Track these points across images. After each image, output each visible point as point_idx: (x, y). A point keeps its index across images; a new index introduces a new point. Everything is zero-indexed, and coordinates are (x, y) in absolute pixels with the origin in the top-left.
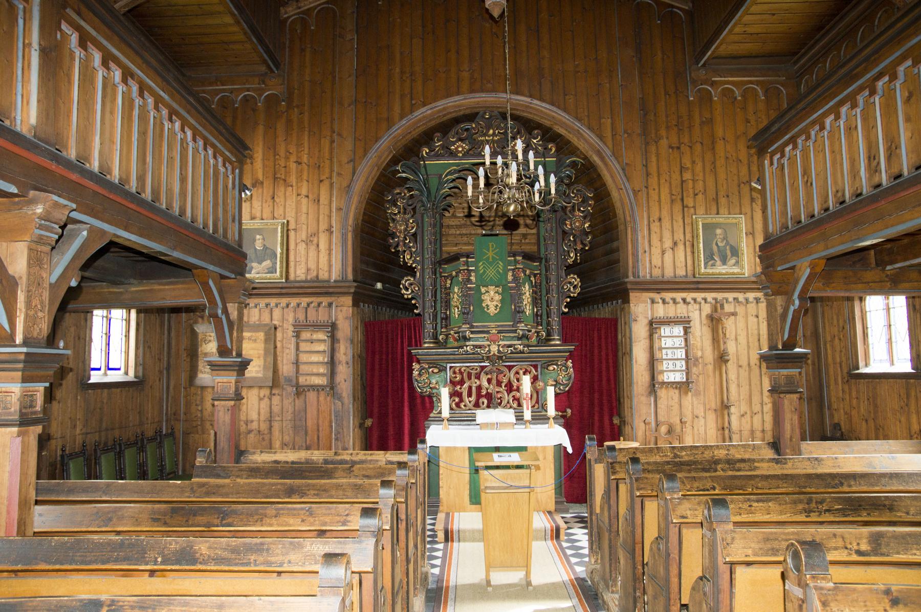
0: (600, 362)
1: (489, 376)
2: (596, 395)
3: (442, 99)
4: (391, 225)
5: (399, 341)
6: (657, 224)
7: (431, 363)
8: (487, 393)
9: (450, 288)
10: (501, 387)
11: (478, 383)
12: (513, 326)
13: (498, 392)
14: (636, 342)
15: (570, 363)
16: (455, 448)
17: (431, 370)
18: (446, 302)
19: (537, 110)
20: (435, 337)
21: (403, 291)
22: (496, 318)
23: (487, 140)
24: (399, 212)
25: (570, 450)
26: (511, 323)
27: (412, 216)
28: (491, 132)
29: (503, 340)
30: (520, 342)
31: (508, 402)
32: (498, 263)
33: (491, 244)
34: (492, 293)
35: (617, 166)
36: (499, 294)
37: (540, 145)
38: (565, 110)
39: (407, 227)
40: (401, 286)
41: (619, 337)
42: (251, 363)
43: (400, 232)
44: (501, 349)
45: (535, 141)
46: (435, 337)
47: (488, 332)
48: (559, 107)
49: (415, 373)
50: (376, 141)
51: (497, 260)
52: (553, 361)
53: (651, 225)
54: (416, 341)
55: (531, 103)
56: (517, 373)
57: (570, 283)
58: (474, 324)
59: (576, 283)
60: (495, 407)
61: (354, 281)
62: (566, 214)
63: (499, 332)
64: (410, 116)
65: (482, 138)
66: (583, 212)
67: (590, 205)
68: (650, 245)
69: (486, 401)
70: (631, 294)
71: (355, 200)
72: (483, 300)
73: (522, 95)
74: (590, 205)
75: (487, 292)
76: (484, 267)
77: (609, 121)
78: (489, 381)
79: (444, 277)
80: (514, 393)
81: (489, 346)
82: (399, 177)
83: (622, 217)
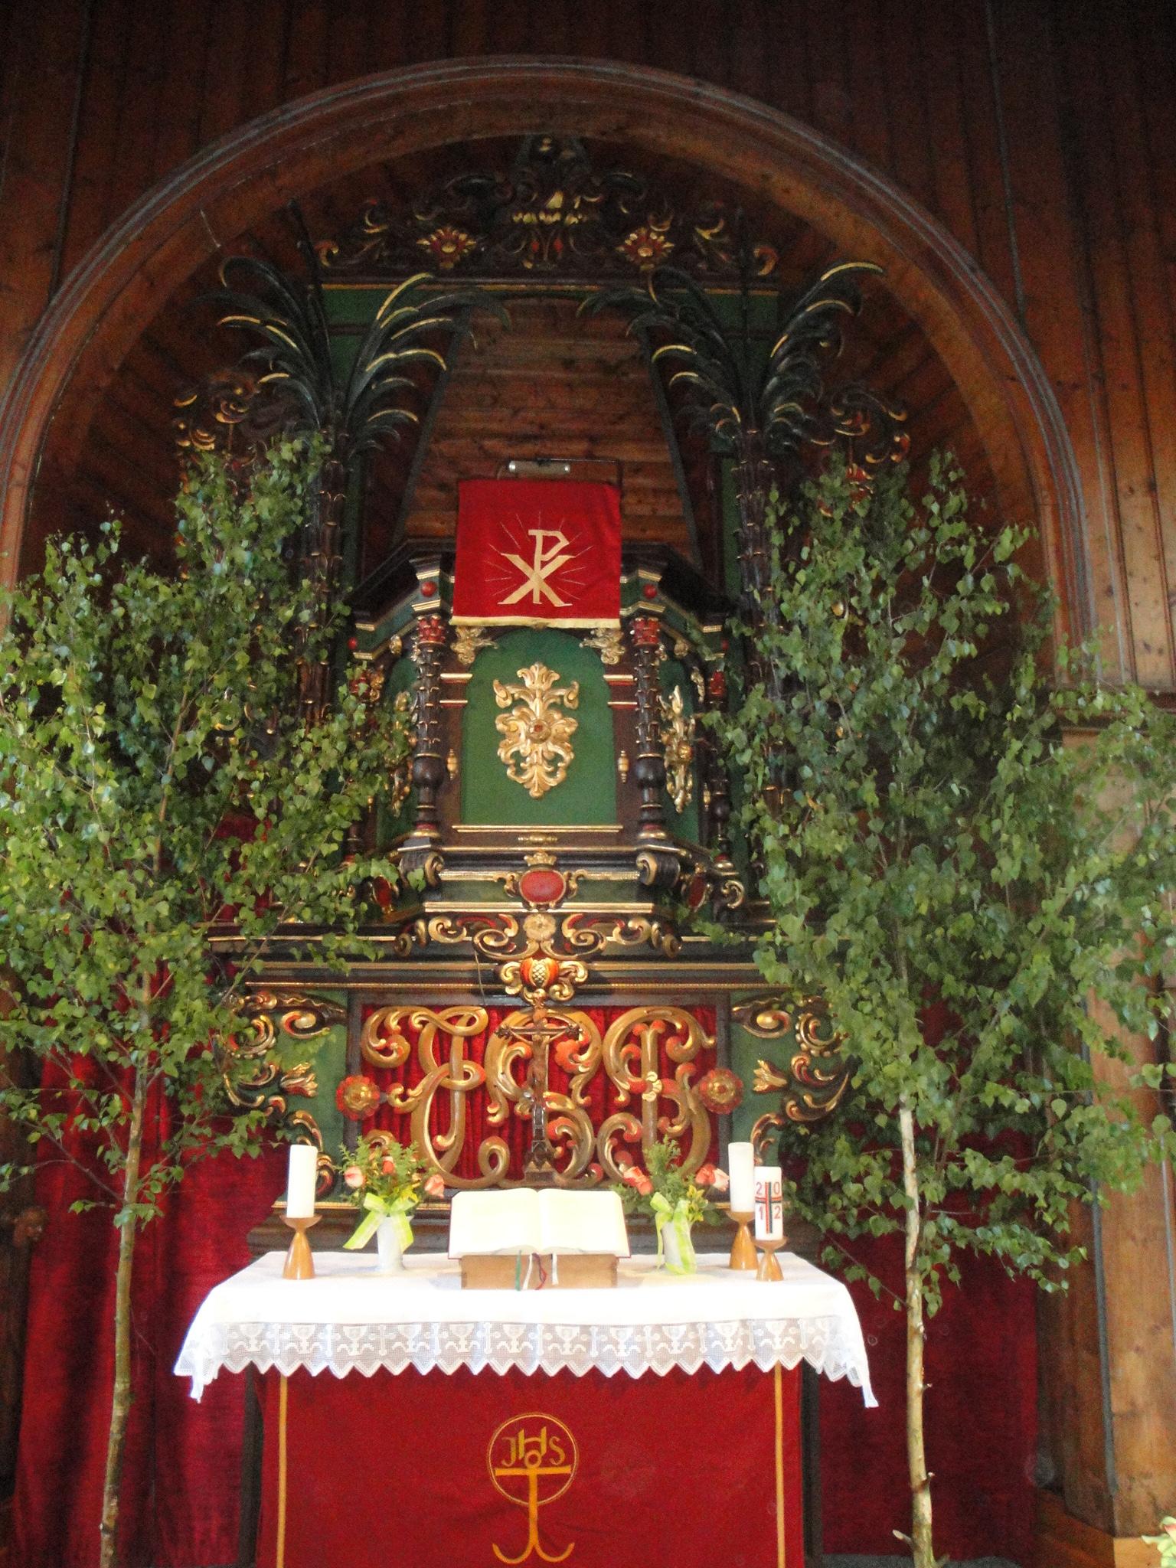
6: (1141, 499)
10: (569, 1093)
11: (475, 1078)
12: (618, 839)
13: (553, 1115)
22: (547, 807)
26: (614, 828)
28: (556, 201)
29: (580, 897)
30: (647, 907)
31: (595, 1158)
34: (536, 706)
37: (722, 247)
42: (1164, 976)
44: (569, 933)
45: (706, 235)
47: (513, 860)
53: (1122, 500)
55: (696, 95)
56: (631, 1038)
58: (462, 829)
60: (541, 1182)
63: (566, 861)
64: (276, 112)
67: (897, 448)
68: (1124, 572)
71: (52, 381)
72: (502, 736)
74: (897, 448)
75: (518, 703)
78: (519, 1067)
81: (520, 918)
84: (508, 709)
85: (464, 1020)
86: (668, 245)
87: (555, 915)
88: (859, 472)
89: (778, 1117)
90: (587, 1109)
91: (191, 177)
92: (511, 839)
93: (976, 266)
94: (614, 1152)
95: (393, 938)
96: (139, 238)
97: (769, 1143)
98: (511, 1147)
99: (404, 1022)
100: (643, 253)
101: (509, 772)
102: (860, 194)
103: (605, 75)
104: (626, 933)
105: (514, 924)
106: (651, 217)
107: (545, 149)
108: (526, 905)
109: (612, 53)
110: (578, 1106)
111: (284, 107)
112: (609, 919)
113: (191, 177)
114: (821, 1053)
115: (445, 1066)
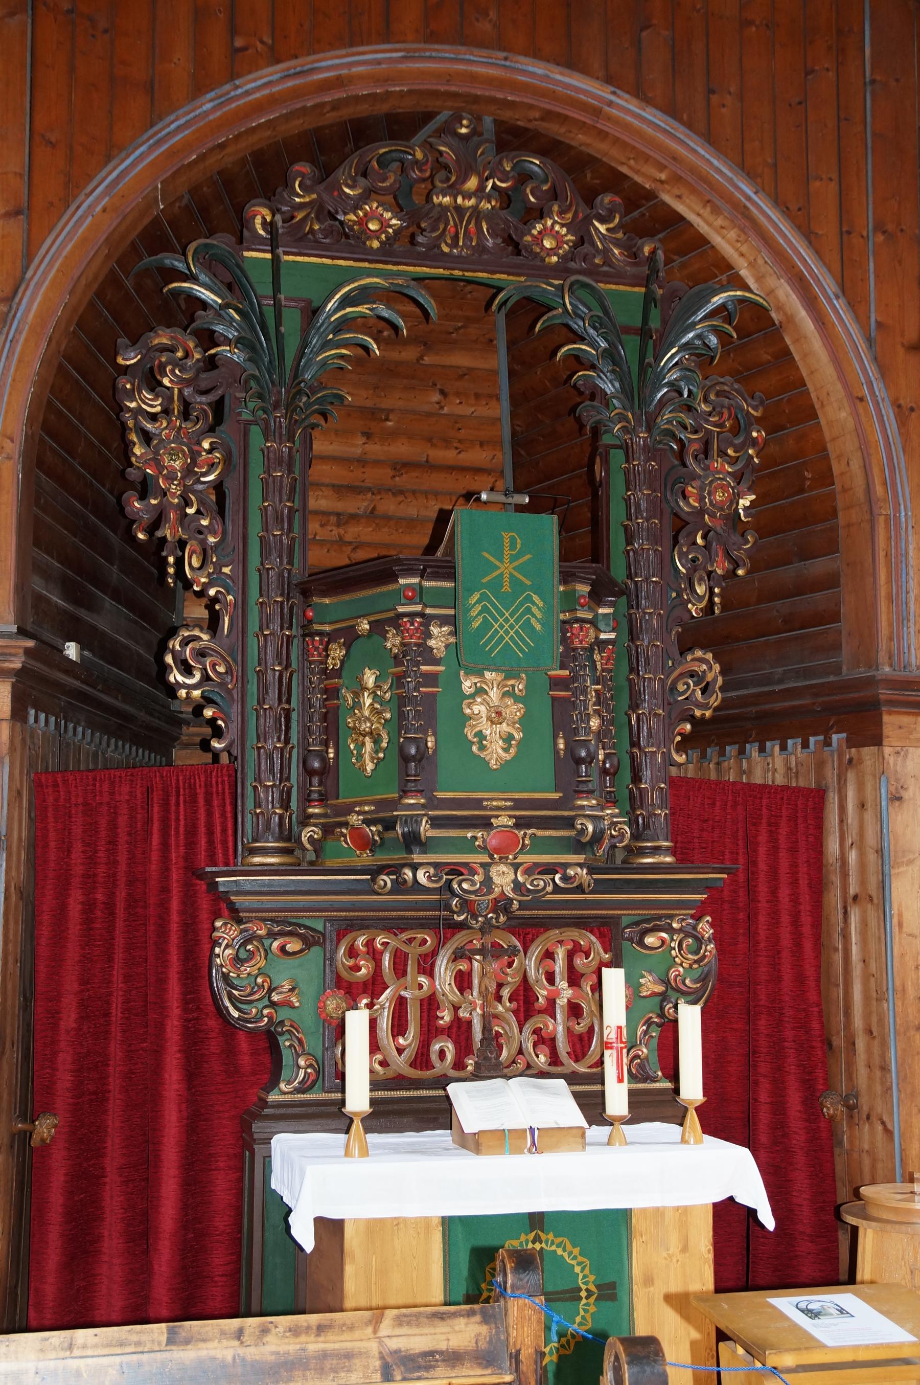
0: (774, 915)
1: (463, 966)
2: (763, 1023)
3: (332, 46)
4: (138, 451)
5: (156, 840)
7: (273, 920)
8: (457, 1020)
9: (338, 673)
14: (899, 865)
15: (705, 928)
16: (397, 1223)
17: (276, 944)
18: (325, 717)
19: (627, 127)
20: (288, 836)
21: (176, 676)
23: (459, 209)
24: (166, 411)
25: (768, 1221)
26: (556, 796)
27: (211, 430)
28: (472, 183)
30: (581, 858)
31: (520, 1052)
32: (529, 599)
33: (506, 537)
34: (494, 694)
35: (854, 329)
36: (517, 699)
38: (710, 138)
39: (194, 463)
40: (169, 659)
41: (832, 846)
43: (170, 478)
45: (602, 228)
46: (288, 836)
47: (485, 823)
48: (690, 126)
49: (223, 954)
50: (109, 158)
51: (525, 588)
52: (659, 918)
54: (226, 854)
55: (610, 104)
57: (692, 674)
59: (710, 677)
61: (22, 632)
62: (684, 465)
63: (521, 823)
64: (227, 87)
65: (447, 200)
66: (733, 461)
69: (450, 1048)
70: (886, 718)
73: (584, 70)
74: (754, 443)
75: (480, 691)
76: (485, 609)
77: (833, 187)
78: (463, 981)
79: (321, 634)
80: (537, 1021)
81: (486, 866)
82: (177, 293)
83: (859, 483)
84: (473, 696)
85: (417, 942)
86: (570, 237)
87: (512, 864)
88: (723, 465)
89: (658, 1016)
90: (516, 1012)
91: (151, 149)
92: (477, 804)
93: (840, 294)
94: (535, 1045)
95: (369, 877)
96: (104, 210)
97: (652, 1037)
98: (456, 1043)
99: (369, 944)
100: (547, 244)
101: (475, 748)
102: (745, 212)
103: (533, 75)
104: (565, 878)
105: (481, 871)
106: (556, 208)
107: (464, 131)
108: (491, 857)
109: (535, 53)
110: (507, 1010)
111: (237, 82)
112: (550, 869)
113: (151, 149)
114: (691, 966)
115: (402, 980)
